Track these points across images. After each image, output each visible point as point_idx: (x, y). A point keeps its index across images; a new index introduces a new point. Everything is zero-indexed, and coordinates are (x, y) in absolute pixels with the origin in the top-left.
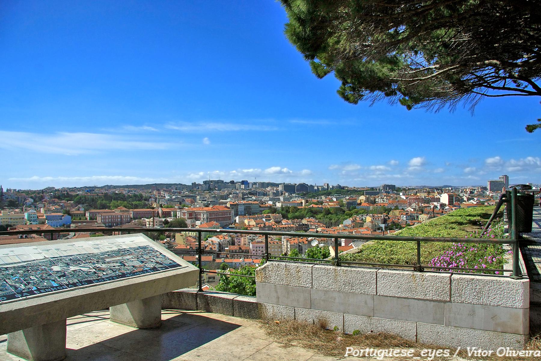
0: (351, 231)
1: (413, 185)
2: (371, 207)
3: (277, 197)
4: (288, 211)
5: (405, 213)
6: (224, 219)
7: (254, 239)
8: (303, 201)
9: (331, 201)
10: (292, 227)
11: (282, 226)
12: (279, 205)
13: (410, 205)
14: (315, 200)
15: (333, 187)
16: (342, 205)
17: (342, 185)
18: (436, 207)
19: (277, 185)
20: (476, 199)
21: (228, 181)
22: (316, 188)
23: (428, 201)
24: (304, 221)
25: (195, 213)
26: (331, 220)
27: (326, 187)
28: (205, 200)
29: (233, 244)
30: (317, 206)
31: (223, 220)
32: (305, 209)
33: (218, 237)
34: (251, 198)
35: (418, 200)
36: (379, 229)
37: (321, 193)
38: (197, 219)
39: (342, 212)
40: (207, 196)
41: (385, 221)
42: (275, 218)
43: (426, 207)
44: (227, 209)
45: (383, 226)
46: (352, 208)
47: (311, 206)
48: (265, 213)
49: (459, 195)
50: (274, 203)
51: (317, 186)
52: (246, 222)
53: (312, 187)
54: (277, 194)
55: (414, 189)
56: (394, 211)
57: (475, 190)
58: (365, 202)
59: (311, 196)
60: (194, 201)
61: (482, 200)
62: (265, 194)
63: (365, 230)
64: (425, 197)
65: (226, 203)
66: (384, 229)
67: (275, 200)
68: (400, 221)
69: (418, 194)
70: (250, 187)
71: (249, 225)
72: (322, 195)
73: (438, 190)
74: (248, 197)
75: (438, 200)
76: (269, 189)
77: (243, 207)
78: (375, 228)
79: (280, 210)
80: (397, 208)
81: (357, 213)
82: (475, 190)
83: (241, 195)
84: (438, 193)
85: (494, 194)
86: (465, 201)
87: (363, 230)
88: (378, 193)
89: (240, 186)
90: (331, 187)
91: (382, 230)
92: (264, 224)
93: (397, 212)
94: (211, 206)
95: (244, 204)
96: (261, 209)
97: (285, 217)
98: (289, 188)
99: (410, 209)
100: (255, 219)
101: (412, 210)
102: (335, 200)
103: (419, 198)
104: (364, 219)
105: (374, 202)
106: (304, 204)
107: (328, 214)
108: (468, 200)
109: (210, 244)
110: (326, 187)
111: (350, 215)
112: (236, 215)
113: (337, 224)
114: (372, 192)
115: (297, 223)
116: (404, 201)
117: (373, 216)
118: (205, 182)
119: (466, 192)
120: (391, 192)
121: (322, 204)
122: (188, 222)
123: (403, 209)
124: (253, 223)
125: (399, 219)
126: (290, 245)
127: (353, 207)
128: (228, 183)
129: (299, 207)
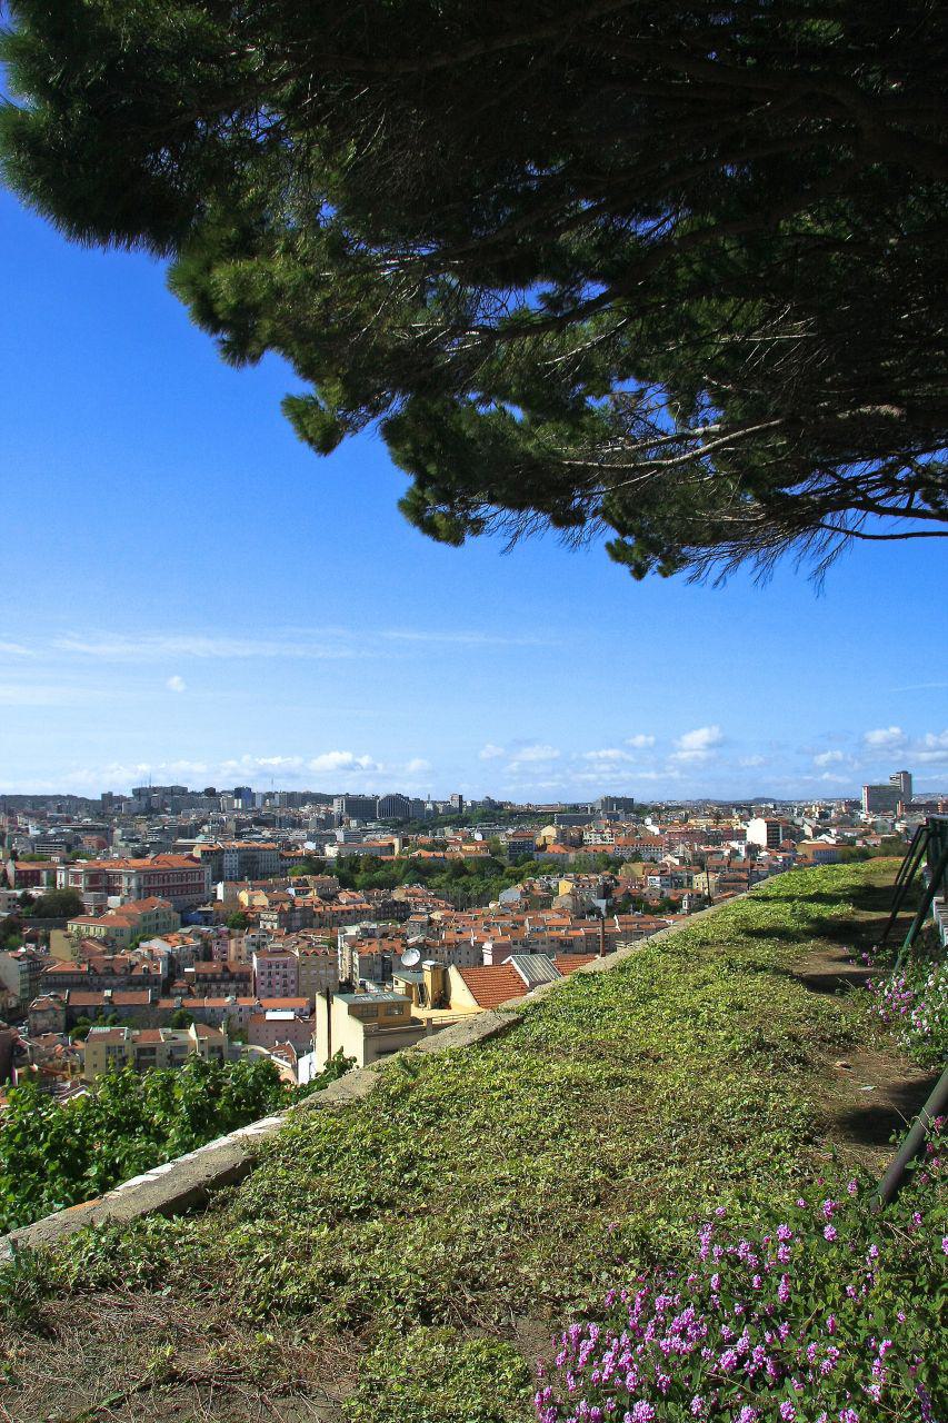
0: (520, 917)
2: (572, 856)
4: (354, 869)
5: (657, 871)
6: (185, 889)
7: (264, 944)
8: (396, 842)
9: (469, 840)
10: (367, 910)
12: (331, 852)
13: (671, 848)
14: (426, 839)
16: (497, 852)
17: (498, 798)
18: (735, 853)
19: (328, 799)
21: (200, 789)
22: (429, 807)
23: (715, 839)
24: (398, 895)
25: (107, 874)
26: (467, 889)
27: (456, 804)
28: (137, 841)
29: (207, 955)
30: (432, 854)
31: (178, 895)
32: (400, 861)
35: (691, 835)
36: (591, 913)
37: (443, 819)
38: (113, 891)
41: (606, 892)
42: (321, 888)
43: (712, 853)
44: (193, 864)
45: (602, 904)
46: (521, 861)
47: (416, 854)
48: (293, 874)
49: (793, 823)
51: (434, 803)
52: (244, 897)
53: (419, 803)
55: (679, 808)
56: (631, 865)
57: (830, 808)
58: (556, 841)
59: (416, 827)
60: (106, 842)
61: (849, 835)
62: (297, 824)
63: (557, 916)
65: (191, 848)
67: (322, 839)
68: (644, 891)
69: (692, 821)
70: (258, 804)
71: (252, 907)
73: (741, 809)
75: (741, 835)
76: (306, 809)
78: (580, 910)
80: (637, 857)
81: (535, 871)
83: (232, 826)
84: (742, 819)
85: (879, 819)
88: (589, 820)
89: (231, 802)
90: (469, 804)
91: (599, 915)
92: (293, 902)
93: (638, 868)
95: (239, 850)
97: (346, 883)
98: (360, 807)
100: (268, 890)
101: (677, 862)
102: (478, 837)
105: (579, 843)
109: (144, 959)
110: (456, 804)
111: (518, 878)
112: (218, 878)
113: (483, 900)
114: (573, 816)
116: (656, 840)
118: (138, 793)
120: (622, 816)
122: (88, 899)
123: (652, 860)
124: (261, 900)
126: (361, 959)
128: (199, 794)
129: (384, 858)
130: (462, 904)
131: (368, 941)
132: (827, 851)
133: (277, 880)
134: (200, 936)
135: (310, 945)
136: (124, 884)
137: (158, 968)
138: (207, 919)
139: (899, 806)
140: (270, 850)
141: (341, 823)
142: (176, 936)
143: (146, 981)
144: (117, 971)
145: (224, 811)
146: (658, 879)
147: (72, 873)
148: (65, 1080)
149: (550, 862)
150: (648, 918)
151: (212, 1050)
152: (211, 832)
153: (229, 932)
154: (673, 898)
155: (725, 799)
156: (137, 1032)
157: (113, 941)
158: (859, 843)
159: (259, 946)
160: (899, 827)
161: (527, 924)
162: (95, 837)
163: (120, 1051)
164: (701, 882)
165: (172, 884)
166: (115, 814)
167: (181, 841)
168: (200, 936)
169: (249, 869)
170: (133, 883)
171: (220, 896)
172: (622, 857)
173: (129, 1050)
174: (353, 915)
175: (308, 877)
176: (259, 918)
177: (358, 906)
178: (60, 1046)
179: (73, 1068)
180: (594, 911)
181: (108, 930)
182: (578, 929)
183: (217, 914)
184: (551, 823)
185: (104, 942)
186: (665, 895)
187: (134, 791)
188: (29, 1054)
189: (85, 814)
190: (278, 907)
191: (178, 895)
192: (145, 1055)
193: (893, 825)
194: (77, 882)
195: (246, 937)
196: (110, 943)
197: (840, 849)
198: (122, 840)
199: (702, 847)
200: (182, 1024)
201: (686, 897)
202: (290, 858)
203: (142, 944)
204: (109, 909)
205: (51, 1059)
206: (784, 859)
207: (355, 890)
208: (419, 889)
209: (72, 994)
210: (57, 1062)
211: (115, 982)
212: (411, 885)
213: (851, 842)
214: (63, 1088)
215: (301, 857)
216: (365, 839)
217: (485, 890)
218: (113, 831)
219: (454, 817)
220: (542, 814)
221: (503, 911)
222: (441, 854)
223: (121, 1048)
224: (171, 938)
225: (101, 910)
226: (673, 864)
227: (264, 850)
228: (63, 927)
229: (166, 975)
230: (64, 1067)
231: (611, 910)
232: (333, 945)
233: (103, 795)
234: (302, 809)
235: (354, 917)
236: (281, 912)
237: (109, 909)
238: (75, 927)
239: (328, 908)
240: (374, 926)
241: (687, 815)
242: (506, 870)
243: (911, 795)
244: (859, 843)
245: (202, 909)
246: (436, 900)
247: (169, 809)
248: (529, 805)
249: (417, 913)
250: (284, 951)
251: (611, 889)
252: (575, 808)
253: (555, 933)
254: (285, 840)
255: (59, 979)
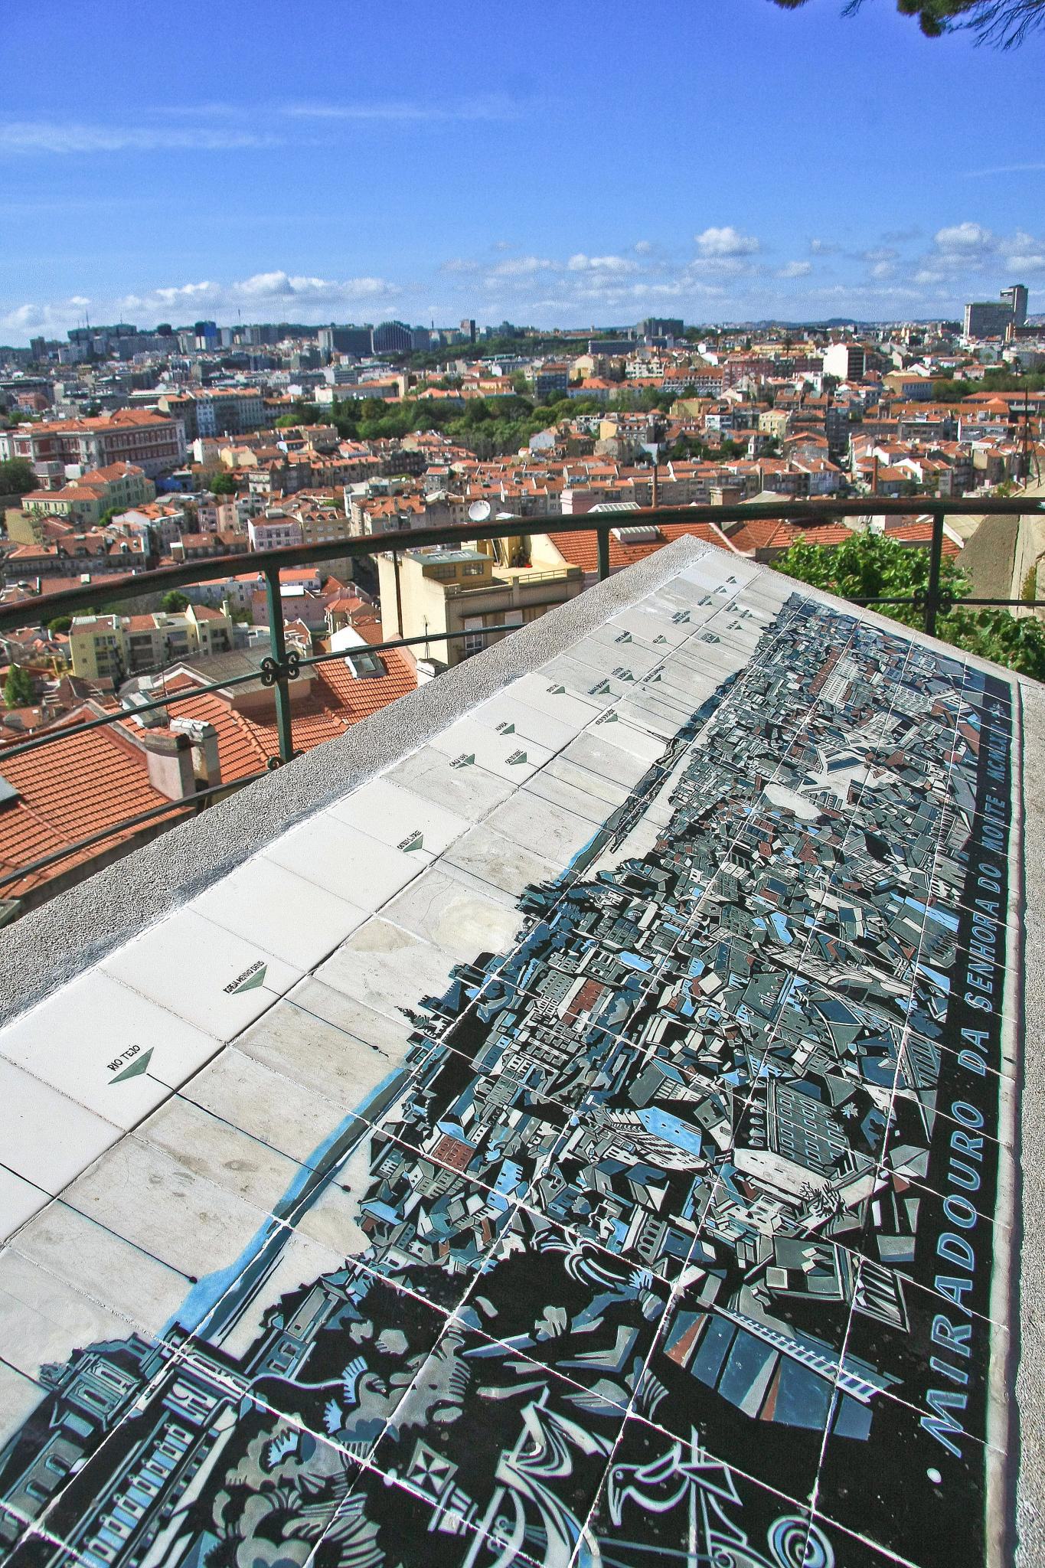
0: (557, 466)
1: (738, 320)
2: (613, 393)
3: (315, 371)
4: (355, 416)
5: (716, 408)
6: (155, 451)
7: (259, 510)
8: (401, 381)
9: (486, 375)
11: (341, 463)
12: (323, 397)
13: (732, 381)
14: (437, 376)
15: (489, 330)
16: (523, 389)
17: (518, 323)
18: (809, 387)
19: (311, 332)
20: (927, 360)
21: (153, 326)
22: (435, 336)
24: (409, 444)
25: (60, 438)
26: (491, 435)
27: (466, 332)
28: (84, 396)
29: (193, 527)
30: (445, 394)
31: (149, 459)
32: (408, 405)
33: (144, 512)
34: (236, 378)
35: (758, 366)
37: (453, 351)
38: (72, 459)
39: (520, 411)
40: (89, 379)
41: (657, 434)
42: (317, 439)
43: (782, 387)
44: (159, 420)
45: (652, 449)
47: (427, 394)
48: (282, 425)
49: (878, 350)
50: (306, 391)
51: (440, 331)
52: (226, 455)
53: (423, 332)
54: (312, 361)
55: (739, 332)
57: (924, 332)
58: (594, 375)
59: (421, 361)
60: (46, 398)
61: (946, 365)
62: (275, 364)
63: (601, 464)
64: (777, 356)
65: (154, 400)
66: (655, 459)
67: (310, 381)
68: (702, 432)
69: (756, 348)
70: (226, 342)
71: (238, 467)
72: (458, 357)
74: (223, 377)
75: (817, 365)
76: (286, 345)
77: (210, 409)
78: (627, 456)
79: (331, 413)
80: (691, 392)
81: (571, 412)
82: (924, 332)
83: (197, 371)
84: (818, 345)
85: (982, 346)
86: (897, 369)
87: (592, 465)
88: (631, 347)
89: (192, 341)
90: (483, 331)
91: (650, 462)
92: (286, 459)
93: (692, 406)
94: (106, 414)
95: (214, 400)
96: (269, 412)
97: (347, 432)
98: (352, 341)
99: (732, 395)
100: (255, 445)
101: (739, 398)
102: (497, 371)
103: (758, 361)
104: (593, 428)
105: (620, 376)
106: (402, 391)
107: (481, 420)
108: (905, 366)
109: (120, 536)
110: (466, 332)
111: (550, 420)
112: (192, 436)
113: (511, 447)
114: (612, 343)
115: (386, 449)
116: (714, 372)
117: (621, 420)
118: (76, 336)
119: (898, 340)
120: (670, 343)
121: (459, 387)
122: (42, 471)
123: (710, 395)
124: (248, 458)
125: (698, 427)
126: (373, 522)
127: (557, 394)
128: (151, 334)
129: (388, 400)
130: (487, 453)
131: (382, 500)
132: (918, 385)
133: (264, 433)
134: (182, 505)
135: (314, 509)
136: (82, 449)
137: (138, 545)
138: (185, 485)
139: (1008, 330)
140: (251, 397)
141: (329, 360)
142: (154, 506)
143: (127, 560)
144: (92, 551)
145: (185, 353)
146: (718, 418)
147: (17, 440)
148: (52, 679)
149: (587, 399)
150: (707, 464)
151: (215, 634)
152: (173, 379)
153: (216, 499)
154: (737, 441)
155: (794, 321)
156: (127, 620)
157: (80, 517)
158: (958, 376)
159: (253, 513)
160: (1008, 356)
161: (565, 472)
162: (32, 395)
163: (111, 642)
164: (773, 421)
165: (138, 445)
166: (51, 365)
167: (137, 393)
168: (182, 505)
169: (228, 422)
170: (93, 448)
171: (199, 457)
172: (673, 393)
173: (120, 640)
174: (358, 470)
175: (301, 428)
176: (247, 480)
177: (363, 460)
178: (39, 642)
179: (59, 665)
180: (643, 457)
181: (72, 506)
182: (626, 478)
183: (198, 478)
184: (584, 352)
185: (69, 519)
186: (727, 437)
187: (70, 334)
188: (7, 653)
189: (15, 367)
190: (269, 465)
191: (149, 459)
192: (139, 644)
193: (1000, 354)
194: (24, 450)
195: (236, 503)
196: (77, 519)
197: (935, 382)
198: (66, 396)
199: (770, 380)
200: (175, 607)
201: (752, 439)
202: (275, 406)
203: (115, 519)
204: (68, 480)
205: (33, 657)
206: (867, 394)
207: (359, 441)
208: (435, 436)
209: (44, 582)
210: (40, 659)
211: (91, 565)
212: (424, 433)
213: (948, 374)
214: (52, 688)
215: (288, 404)
216: (360, 380)
217: (512, 436)
218: (52, 386)
219: (466, 347)
220: (572, 342)
221: (537, 460)
222: (457, 393)
223: (111, 639)
224: (149, 509)
225: (59, 482)
226: (734, 401)
227: (244, 397)
228: (19, 505)
229: (148, 553)
230: (49, 664)
231: (664, 457)
232: (339, 505)
233: (33, 342)
234: (280, 346)
235: (361, 472)
236: (273, 471)
237: (68, 480)
238: (32, 505)
239: (328, 464)
240: (385, 482)
241: (749, 341)
242: (536, 410)
243: (1024, 316)
244: (958, 376)
245: (178, 473)
246: (456, 449)
247: (117, 355)
248: (556, 330)
249: (433, 465)
250: (285, 516)
251: (664, 431)
252: (612, 333)
253: (599, 484)
254: (264, 386)
255: (26, 566)
